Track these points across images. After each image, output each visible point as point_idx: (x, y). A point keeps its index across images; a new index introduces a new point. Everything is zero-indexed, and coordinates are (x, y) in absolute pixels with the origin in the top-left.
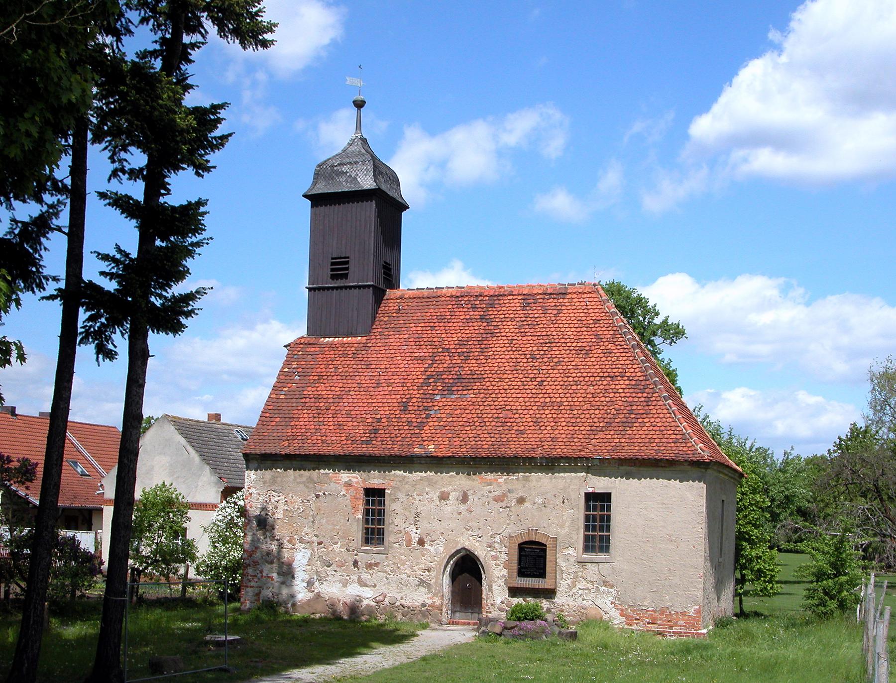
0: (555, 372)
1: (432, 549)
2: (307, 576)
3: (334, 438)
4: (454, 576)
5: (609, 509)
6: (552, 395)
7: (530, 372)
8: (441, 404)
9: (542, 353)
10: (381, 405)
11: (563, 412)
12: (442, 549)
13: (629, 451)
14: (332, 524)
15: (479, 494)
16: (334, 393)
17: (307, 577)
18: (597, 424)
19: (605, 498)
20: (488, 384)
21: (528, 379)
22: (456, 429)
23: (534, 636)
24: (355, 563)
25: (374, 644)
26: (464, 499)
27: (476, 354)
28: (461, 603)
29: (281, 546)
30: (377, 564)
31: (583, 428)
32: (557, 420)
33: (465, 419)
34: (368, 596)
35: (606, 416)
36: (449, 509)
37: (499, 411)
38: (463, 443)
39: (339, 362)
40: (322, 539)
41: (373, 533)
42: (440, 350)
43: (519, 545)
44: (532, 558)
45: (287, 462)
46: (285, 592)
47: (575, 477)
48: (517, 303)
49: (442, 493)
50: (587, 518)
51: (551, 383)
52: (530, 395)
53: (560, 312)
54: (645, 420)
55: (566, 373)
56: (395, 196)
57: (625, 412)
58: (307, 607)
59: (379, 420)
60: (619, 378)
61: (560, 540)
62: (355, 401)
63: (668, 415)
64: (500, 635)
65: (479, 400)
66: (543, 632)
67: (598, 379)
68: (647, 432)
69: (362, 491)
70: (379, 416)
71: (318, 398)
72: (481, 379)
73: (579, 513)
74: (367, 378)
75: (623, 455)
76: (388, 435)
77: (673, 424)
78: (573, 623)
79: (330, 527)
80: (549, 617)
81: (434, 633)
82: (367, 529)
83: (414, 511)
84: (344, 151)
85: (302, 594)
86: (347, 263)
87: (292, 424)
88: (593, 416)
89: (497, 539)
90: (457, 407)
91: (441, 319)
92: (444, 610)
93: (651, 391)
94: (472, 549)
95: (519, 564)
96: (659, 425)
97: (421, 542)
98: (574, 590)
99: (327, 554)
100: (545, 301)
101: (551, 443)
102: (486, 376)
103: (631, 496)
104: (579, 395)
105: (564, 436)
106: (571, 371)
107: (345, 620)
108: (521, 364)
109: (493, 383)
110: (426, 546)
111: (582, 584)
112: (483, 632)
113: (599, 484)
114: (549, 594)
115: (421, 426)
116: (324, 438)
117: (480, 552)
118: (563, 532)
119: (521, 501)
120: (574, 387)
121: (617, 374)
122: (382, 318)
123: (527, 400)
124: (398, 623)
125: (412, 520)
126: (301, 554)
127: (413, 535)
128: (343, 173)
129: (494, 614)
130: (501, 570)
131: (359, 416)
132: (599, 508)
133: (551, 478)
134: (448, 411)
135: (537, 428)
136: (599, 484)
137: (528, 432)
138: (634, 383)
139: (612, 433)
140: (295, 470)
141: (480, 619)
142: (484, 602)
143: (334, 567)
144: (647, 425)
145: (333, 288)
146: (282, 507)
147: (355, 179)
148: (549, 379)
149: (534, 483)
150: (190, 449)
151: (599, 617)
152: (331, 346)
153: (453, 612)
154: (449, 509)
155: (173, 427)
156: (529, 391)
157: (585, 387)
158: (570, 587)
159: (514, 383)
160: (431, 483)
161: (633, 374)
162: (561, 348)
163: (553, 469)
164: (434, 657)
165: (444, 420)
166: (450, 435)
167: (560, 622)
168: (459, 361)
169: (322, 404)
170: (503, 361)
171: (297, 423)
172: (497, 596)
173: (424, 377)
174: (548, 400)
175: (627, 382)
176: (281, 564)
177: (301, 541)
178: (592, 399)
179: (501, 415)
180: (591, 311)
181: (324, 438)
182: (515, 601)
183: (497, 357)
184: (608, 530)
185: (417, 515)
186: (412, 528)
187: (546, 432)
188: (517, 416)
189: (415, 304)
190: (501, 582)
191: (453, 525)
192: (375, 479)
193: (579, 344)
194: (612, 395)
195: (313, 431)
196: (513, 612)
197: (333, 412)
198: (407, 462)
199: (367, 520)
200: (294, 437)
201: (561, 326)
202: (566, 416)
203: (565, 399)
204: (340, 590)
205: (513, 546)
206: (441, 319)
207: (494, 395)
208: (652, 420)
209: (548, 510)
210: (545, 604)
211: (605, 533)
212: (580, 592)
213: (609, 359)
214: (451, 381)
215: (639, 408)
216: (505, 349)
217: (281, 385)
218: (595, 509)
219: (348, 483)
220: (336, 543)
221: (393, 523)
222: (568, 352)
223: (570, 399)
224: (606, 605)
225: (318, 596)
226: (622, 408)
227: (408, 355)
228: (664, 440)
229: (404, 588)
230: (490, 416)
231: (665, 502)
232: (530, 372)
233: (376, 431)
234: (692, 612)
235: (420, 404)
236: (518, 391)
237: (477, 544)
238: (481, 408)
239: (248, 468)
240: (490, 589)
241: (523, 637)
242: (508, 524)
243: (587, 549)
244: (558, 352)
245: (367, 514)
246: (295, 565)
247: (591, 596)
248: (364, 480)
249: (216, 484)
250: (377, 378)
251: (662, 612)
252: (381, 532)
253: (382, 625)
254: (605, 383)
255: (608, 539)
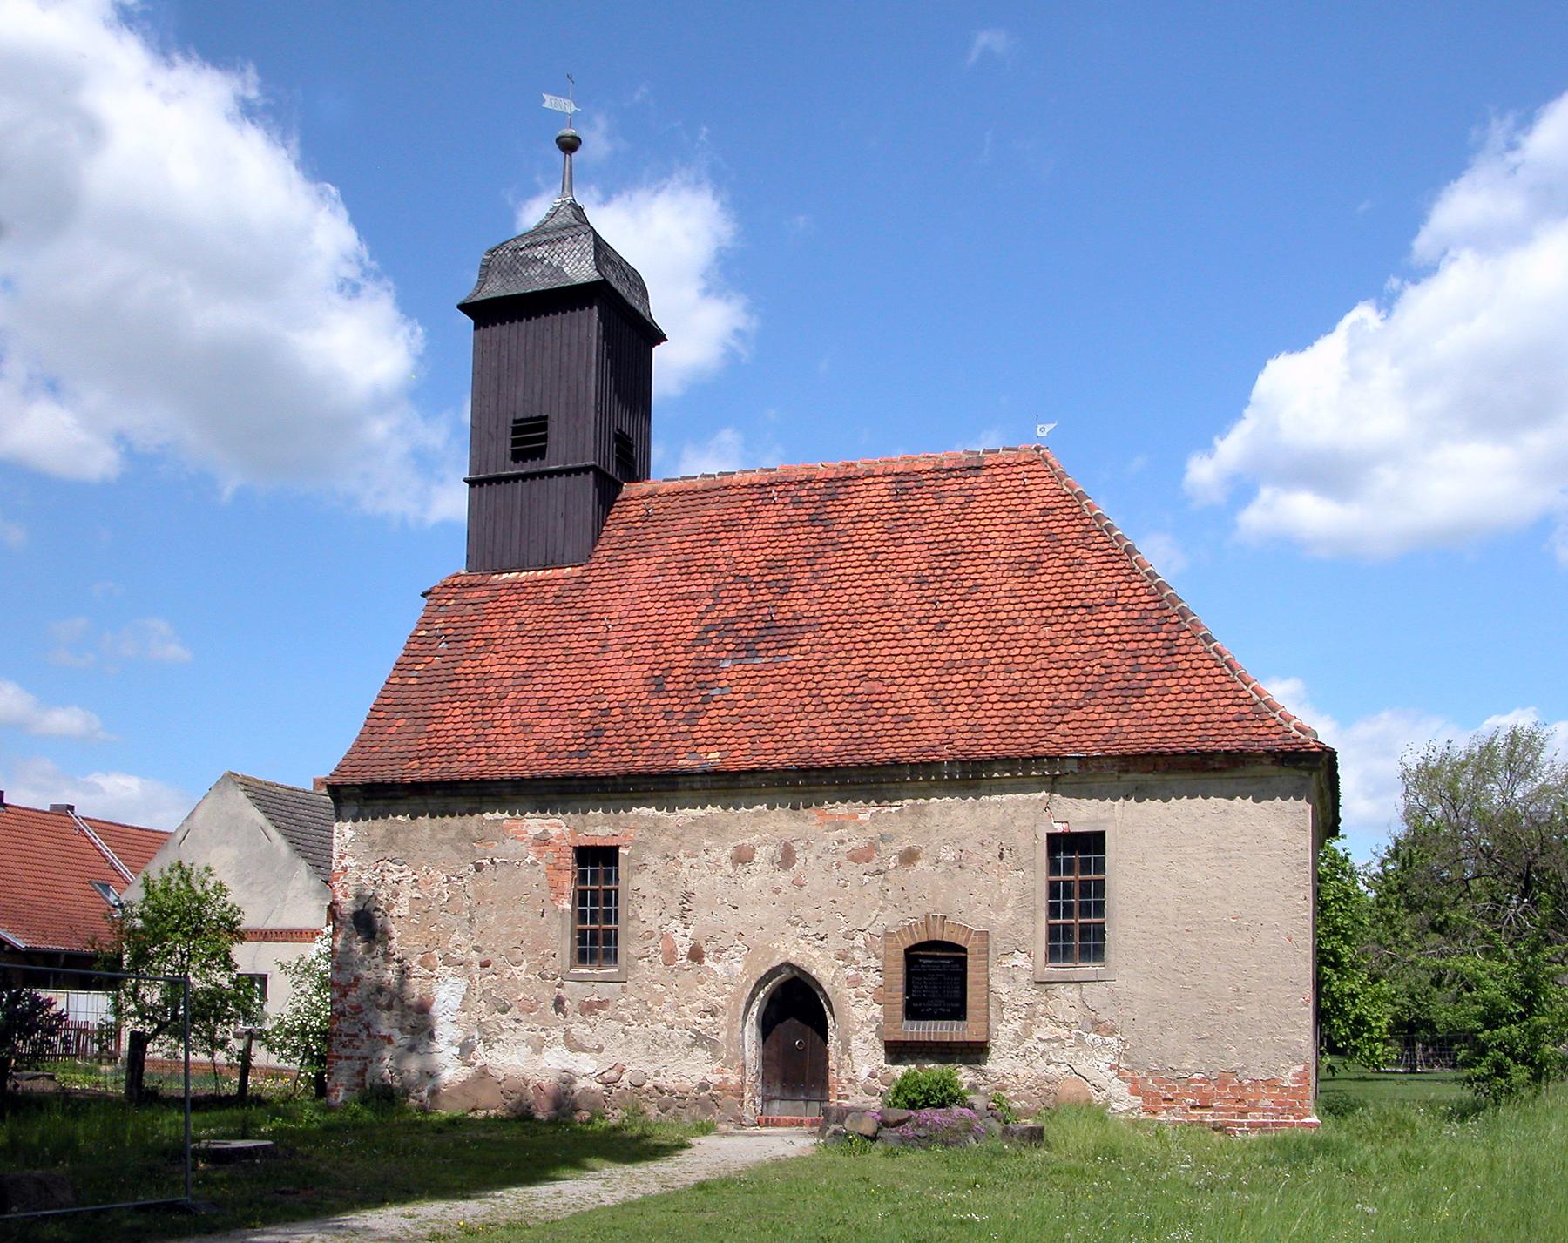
0: (968, 604)
1: (718, 967)
2: (460, 1033)
3: (513, 750)
4: (767, 1025)
5: (1100, 867)
6: (964, 647)
7: (916, 607)
8: (732, 676)
9: (939, 572)
10: (609, 683)
11: (991, 676)
12: (740, 967)
13: (1138, 741)
14: (510, 924)
15: (817, 848)
16: (515, 668)
17: (459, 1035)
18: (1067, 695)
19: (1089, 845)
20: (830, 634)
21: (914, 621)
22: (766, 719)
23: (951, 1138)
24: (559, 1004)
25: (593, 1162)
26: (787, 858)
27: (804, 582)
28: (784, 1080)
29: (404, 973)
30: (603, 1004)
31: (1036, 704)
32: (979, 692)
33: (786, 701)
34: (587, 1070)
35: (1083, 679)
36: (754, 881)
37: (854, 683)
38: (780, 745)
39: (527, 614)
40: (488, 957)
41: (594, 940)
42: (730, 579)
43: (907, 951)
44: (935, 977)
45: (418, 800)
46: (413, 1065)
47: (1025, 803)
48: (882, 490)
49: (739, 849)
50: (1053, 889)
51: (961, 625)
52: (920, 649)
53: (970, 499)
54: (1168, 683)
55: (992, 605)
56: (635, 304)
57: (1123, 669)
58: (460, 1097)
59: (606, 713)
60: (1104, 608)
61: (995, 936)
62: (558, 680)
63: (1217, 671)
64: (874, 1138)
65: (812, 663)
66: (969, 1129)
67: (1059, 612)
68: (1175, 704)
69: (570, 854)
70: (605, 705)
71: (485, 678)
72: (815, 626)
73: (1038, 879)
74: (582, 637)
75: (1130, 748)
76: (623, 739)
77: (1229, 686)
78: (1027, 1114)
79: (505, 930)
80: (979, 1101)
81: (727, 1141)
82: (582, 932)
83: (679, 890)
84: (538, 227)
85: (451, 1072)
86: (544, 427)
87: (429, 728)
88: (1055, 680)
89: (860, 940)
90: (767, 680)
91: (732, 525)
92: (748, 1095)
93: (1175, 628)
94: (805, 966)
95: (908, 991)
96: (1200, 689)
97: (696, 955)
98: (1029, 1043)
99: (501, 986)
100: (940, 482)
101: (969, 735)
102: (825, 619)
103: (1151, 841)
104: (1023, 643)
105: (996, 720)
106: (1002, 601)
107: (538, 1121)
108: (897, 595)
109: (841, 632)
110: (707, 962)
111: (1045, 1030)
112: (836, 1133)
113: (1079, 814)
114: (975, 1052)
115: (691, 718)
116: (492, 751)
117: (823, 970)
118: (1003, 919)
119: (909, 857)
120: (1011, 630)
121: (1098, 601)
122: (614, 530)
123: (912, 658)
124: (649, 1125)
125: (675, 909)
126: (447, 987)
127: (678, 940)
128: (536, 260)
129: (856, 1100)
130: (867, 1007)
131: (565, 707)
132: (1077, 865)
133: (973, 808)
134: (748, 688)
135: (939, 708)
136: (1079, 814)
137: (920, 717)
138: (1136, 615)
139: (1100, 709)
140: (433, 816)
141: (826, 1112)
142: (832, 1076)
143: (515, 1012)
144: (1173, 690)
145: (516, 478)
146: (407, 893)
147: (559, 269)
148: (957, 618)
149: (937, 819)
150: (273, 832)
151: (1083, 1097)
152: (512, 586)
153: (767, 1100)
154: (754, 881)
155: (242, 794)
156: (916, 642)
157: (1033, 629)
158: (1019, 1038)
159: (883, 630)
160: (715, 830)
161: (1133, 600)
162: (977, 562)
163: (976, 787)
164: (726, 1183)
165: (740, 704)
166: (753, 732)
167: (999, 1110)
168: (770, 597)
169: (490, 690)
170: (859, 591)
171: (439, 727)
172: (859, 1062)
173: (697, 629)
174: (957, 656)
175: (1122, 615)
176: (406, 1009)
177: (447, 961)
178: (1051, 650)
179: (858, 690)
180: (1035, 494)
181: (492, 751)
182: (899, 1071)
183: (845, 585)
184: (1100, 909)
185: (687, 896)
186: (676, 926)
187: (957, 715)
188: (893, 689)
189: (678, 503)
190: (869, 1032)
191: (762, 916)
192: (598, 827)
193: (1014, 554)
194: (1091, 640)
195: (472, 739)
196: (899, 1091)
197: (513, 702)
198: (662, 786)
199: (582, 914)
200: (433, 752)
201: (975, 523)
202: (999, 683)
203: (993, 653)
204: (531, 1060)
205: (892, 953)
206: (732, 525)
207: (843, 654)
208: (1184, 681)
209: (968, 875)
210: (964, 1076)
211: (1092, 920)
212: (1042, 1046)
213: (1079, 575)
214: (753, 633)
215: (1152, 660)
216: (862, 570)
217: (411, 660)
218: (1069, 869)
219: (540, 838)
220: (518, 963)
221: (636, 916)
222: (993, 567)
223: (1004, 652)
224: (1099, 1073)
225: (483, 1073)
226: (1117, 662)
227: (665, 591)
228: (1213, 717)
229: (662, 1052)
230: (837, 691)
231: (1222, 846)
232: (916, 607)
233: (599, 733)
234: (1288, 1080)
235: (691, 678)
236: (893, 643)
237: (816, 953)
238: (817, 678)
239: (339, 817)
240: (846, 1048)
241: (925, 1141)
242: (883, 909)
243: (1053, 954)
244: (972, 569)
245: (583, 902)
246: (436, 1009)
247: (1065, 1055)
248: (575, 831)
249: (319, 892)
250: (603, 636)
251: (1223, 1082)
252: (611, 938)
253: (615, 1129)
254: (1075, 618)
255: (1100, 932)
